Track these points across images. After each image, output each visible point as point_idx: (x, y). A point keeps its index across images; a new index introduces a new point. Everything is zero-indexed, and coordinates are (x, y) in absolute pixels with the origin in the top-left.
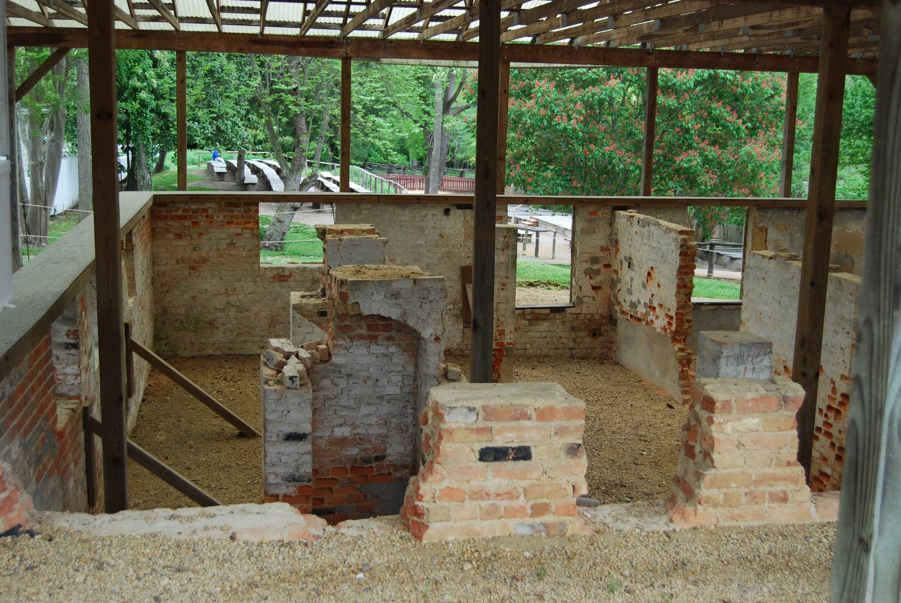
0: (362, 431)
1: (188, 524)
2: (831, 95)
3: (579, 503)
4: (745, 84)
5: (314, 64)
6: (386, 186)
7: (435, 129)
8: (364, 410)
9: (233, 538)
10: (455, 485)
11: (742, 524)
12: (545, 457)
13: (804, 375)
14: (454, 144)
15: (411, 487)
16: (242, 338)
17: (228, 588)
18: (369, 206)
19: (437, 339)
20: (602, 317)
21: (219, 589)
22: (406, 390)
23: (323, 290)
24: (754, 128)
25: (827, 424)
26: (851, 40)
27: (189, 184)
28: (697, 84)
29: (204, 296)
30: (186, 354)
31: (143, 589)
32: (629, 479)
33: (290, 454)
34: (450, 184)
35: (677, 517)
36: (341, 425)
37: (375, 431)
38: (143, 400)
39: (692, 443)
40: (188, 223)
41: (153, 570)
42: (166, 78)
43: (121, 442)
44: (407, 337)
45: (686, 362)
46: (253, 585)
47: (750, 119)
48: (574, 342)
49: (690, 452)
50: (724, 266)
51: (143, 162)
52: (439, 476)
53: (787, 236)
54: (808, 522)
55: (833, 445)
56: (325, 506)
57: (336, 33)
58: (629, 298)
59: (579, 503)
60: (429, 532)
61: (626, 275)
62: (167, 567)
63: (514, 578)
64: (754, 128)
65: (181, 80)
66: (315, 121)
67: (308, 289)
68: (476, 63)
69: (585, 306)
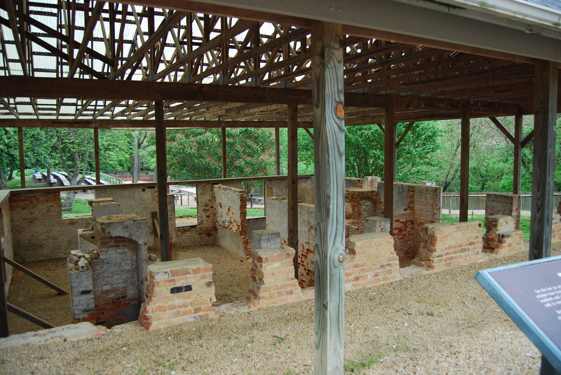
0: (115, 286)
1: (44, 337)
2: (293, 137)
3: (213, 305)
4: (258, 132)
5: (81, 130)
6: (115, 180)
7: (135, 155)
8: (116, 277)
9: (65, 340)
10: (161, 305)
11: (277, 305)
12: (198, 288)
13: (292, 243)
14: (143, 160)
15: (142, 308)
16: (56, 251)
17: (66, 363)
18: (110, 190)
19: (145, 244)
20: (211, 228)
21: (61, 364)
22: (133, 267)
23: (93, 227)
24: (264, 149)
25: (302, 261)
26: (298, 115)
27: (26, 185)
28: (240, 133)
29: (37, 234)
30: (30, 260)
31: (26, 369)
32: (229, 292)
33: (84, 300)
34: (142, 178)
35: (252, 306)
36: (106, 285)
37: (121, 285)
38: (11, 284)
39: (255, 276)
40: (27, 202)
41: (29, 360)
42: (12, 139)
43: (4, 304)
44: (133, 245)
45: (246, 243)
46: (77, 360)
47: (262, 146)
48: (201, 239)
49: (254, 279)
50: (257, 203)
51: (2, 176)
52: (154, 302)
53: (281, 190)
54: (301, 300)
55: (305, 269)
56: (101, 320)
57: (91, 118)
58: (222, 219)
59: (213, 305)
60: (152, 326)
61: (219, 210)
62: (36, 358)
63: (190, 340)
64: (264, 149)
65: (21, 140)
66: (82, 155)
67: (85, 228)
68: (154, 128)
69: (204, 224)
